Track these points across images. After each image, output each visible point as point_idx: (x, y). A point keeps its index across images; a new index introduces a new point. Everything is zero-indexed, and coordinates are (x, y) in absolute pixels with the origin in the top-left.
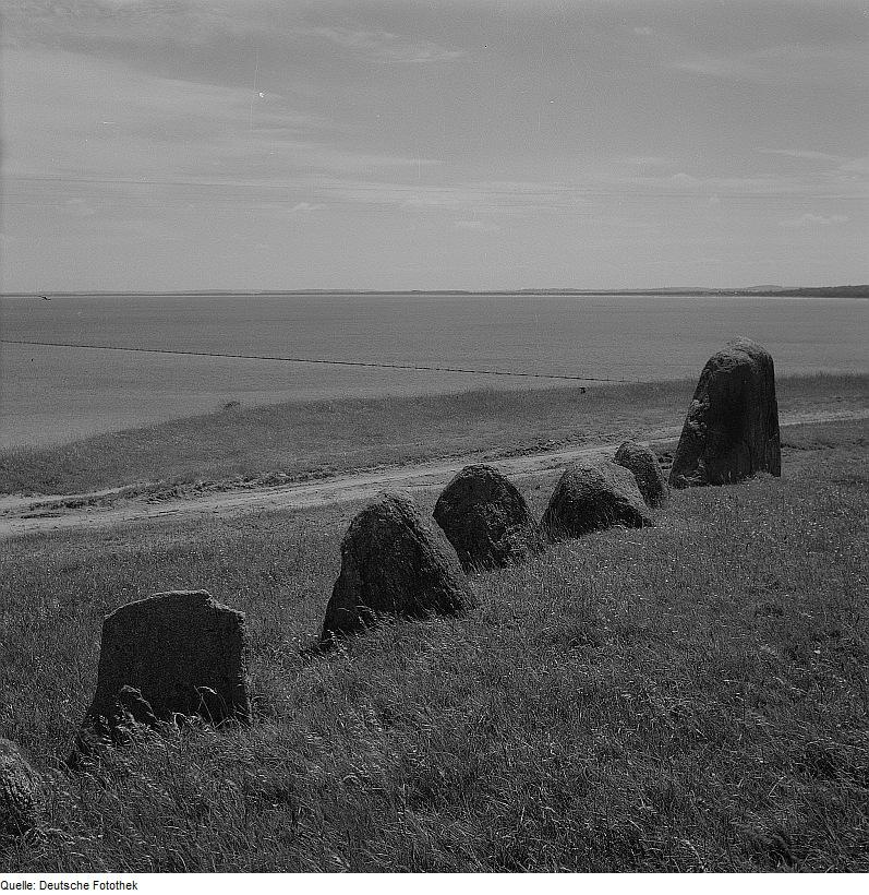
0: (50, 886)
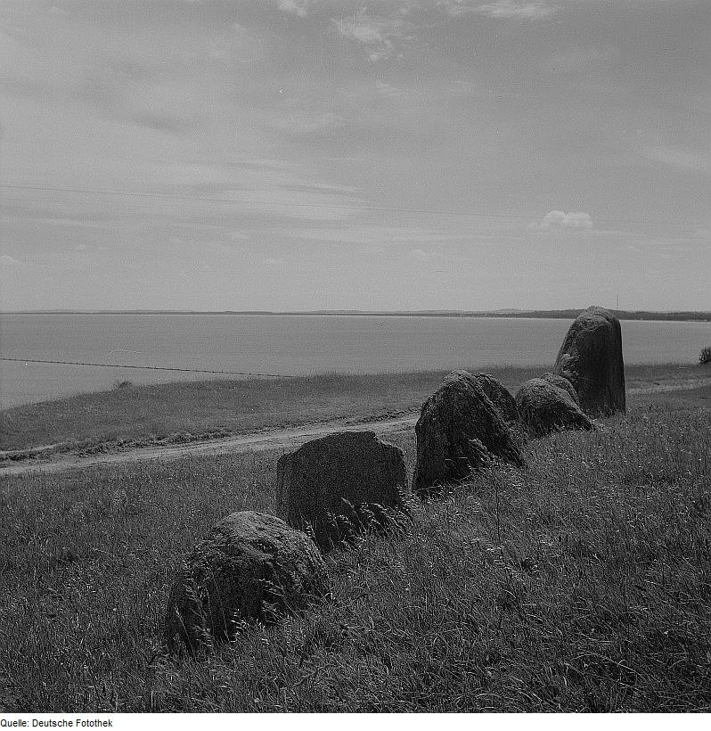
0: (41, 724)
